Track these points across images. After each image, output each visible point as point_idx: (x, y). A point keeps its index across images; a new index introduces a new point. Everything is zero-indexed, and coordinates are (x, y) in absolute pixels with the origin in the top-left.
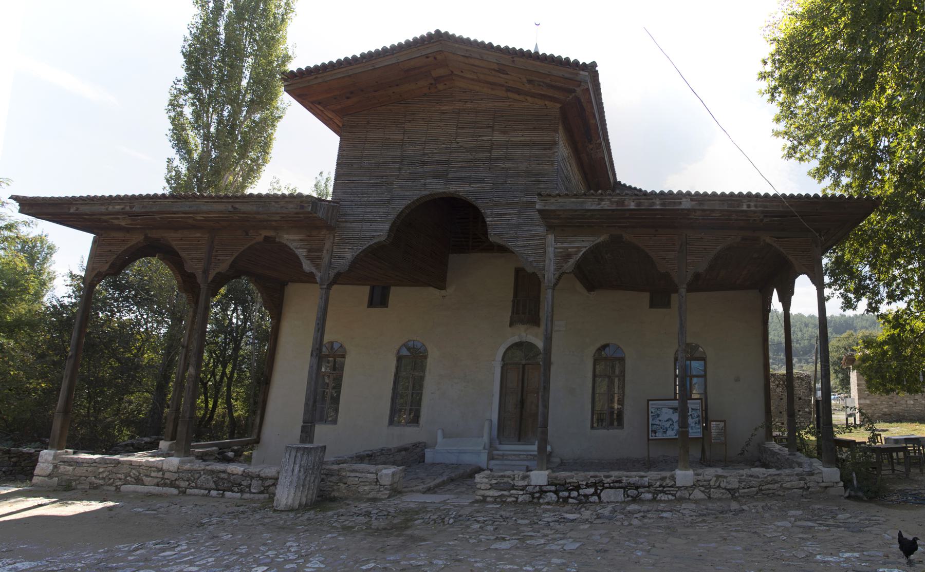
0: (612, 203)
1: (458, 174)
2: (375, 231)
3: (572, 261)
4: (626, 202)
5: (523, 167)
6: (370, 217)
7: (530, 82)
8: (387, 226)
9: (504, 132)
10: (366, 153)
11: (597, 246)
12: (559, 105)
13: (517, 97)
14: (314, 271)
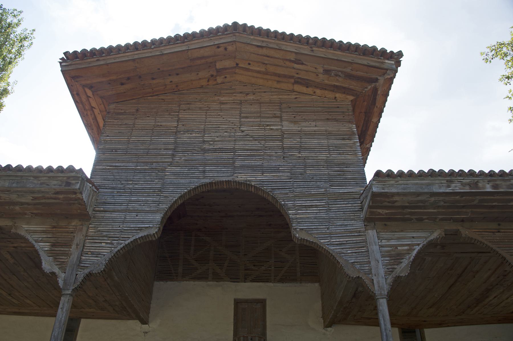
0: (464, 185)
1: (246, 163)
2: (143, 222)
3: (406, 262)
4: (480, 185)
5: (323, 156)
6: (137, 206)
7: (327, 72)
8: (158, 217)
9: (295, 122)
10: (133, 138)
11: (431, 244)
12: (351, 98)
13: (304, 89)
14: (56, 270)
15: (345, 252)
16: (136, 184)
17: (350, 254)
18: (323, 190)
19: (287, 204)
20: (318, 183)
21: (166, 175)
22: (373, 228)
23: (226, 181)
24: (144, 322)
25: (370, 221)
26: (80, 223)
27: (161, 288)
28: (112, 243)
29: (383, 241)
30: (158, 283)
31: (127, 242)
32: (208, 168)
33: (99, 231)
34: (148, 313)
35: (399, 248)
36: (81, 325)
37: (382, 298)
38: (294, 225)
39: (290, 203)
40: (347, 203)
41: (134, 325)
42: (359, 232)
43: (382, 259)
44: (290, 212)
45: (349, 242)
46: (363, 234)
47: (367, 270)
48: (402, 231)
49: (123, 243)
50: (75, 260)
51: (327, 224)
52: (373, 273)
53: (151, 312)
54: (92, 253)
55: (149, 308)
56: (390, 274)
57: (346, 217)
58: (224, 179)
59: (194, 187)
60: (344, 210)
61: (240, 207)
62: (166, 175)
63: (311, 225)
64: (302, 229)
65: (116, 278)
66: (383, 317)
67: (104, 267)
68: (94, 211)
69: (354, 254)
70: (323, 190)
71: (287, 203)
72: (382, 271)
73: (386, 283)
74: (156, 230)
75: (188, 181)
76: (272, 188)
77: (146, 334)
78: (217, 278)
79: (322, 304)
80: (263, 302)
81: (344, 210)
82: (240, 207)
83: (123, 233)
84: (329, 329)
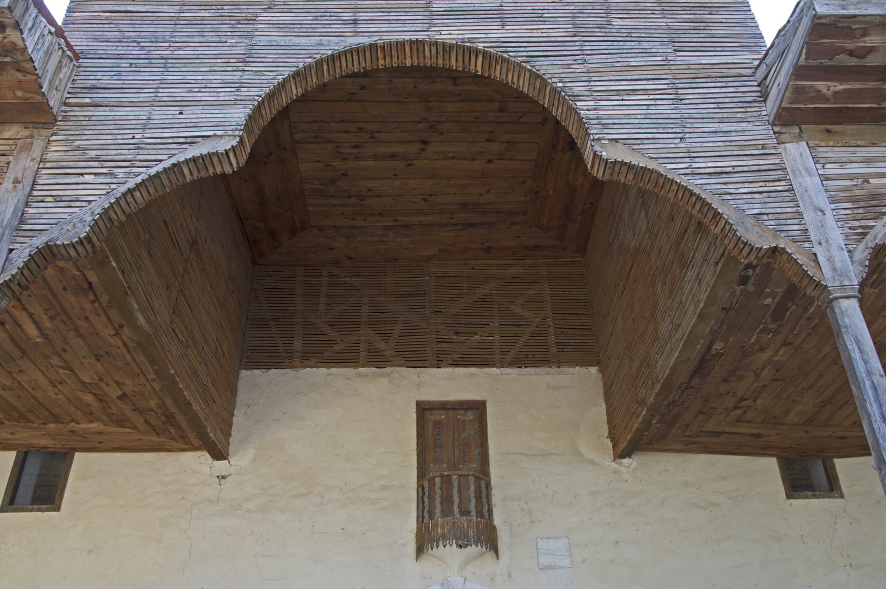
6: (180, 93)
8: (239, 115)
15: (733, 191)
16: (180, 48)
17: (745, 196)
18: (660, 58)
19: (570, 88)
20: (645, 45)
21: (257, 30)
22: (799, 137)
23: (411, 41)
24: (219, 454)
25: (789, 119)
26: (26, 133)
27: (254, 383)
28: (111, 174)
29: (827, 166)
30: (249, 372)
31: (153, 171)
32: (362, 16)
33: (78, 148)
34: (228, 435)
35: (871, 181)
36: (74, 466)
37: (848, 297)
38: (593, 131)
39: (578, 88)
40: (723, 84)
41: (198, 461)
42: (763, 148)
43: (833, 206)
44: (578, 103)
45: (740, 169)
46: (773, 151)
47: (795, 233)
48: (874, 145)
49: (144, 174)
50: (8, 215)
51: (678, 130)
52: (812, 238)
53: (233, 433)
54: (57, 199)
55: (230, 425)
56: (859, 241)
57: (725, 115)
58: (407, 38)
59: (330, 53)
60: (718, 100)
61: (425, 200)
62: (257, 30)
63: (637, 131)
64: (616, 140)
65: (141, 320)
66: (857, 342)
67: (88, 229)
68: (66, 104)
69: (756, 196)
70: (660, 58)
71: (569, 84)
72: (837, 235)
73: (853, 262)
74: (234, 142)
75: (314, 40)
76: (530, 54)
77: (223, 481)
78: (378, 360)
79: (608, 409)
80: (478, 408)
81: (718, 100)
82: (425, 200)
83: (142, 152)
84: (626, 461)
